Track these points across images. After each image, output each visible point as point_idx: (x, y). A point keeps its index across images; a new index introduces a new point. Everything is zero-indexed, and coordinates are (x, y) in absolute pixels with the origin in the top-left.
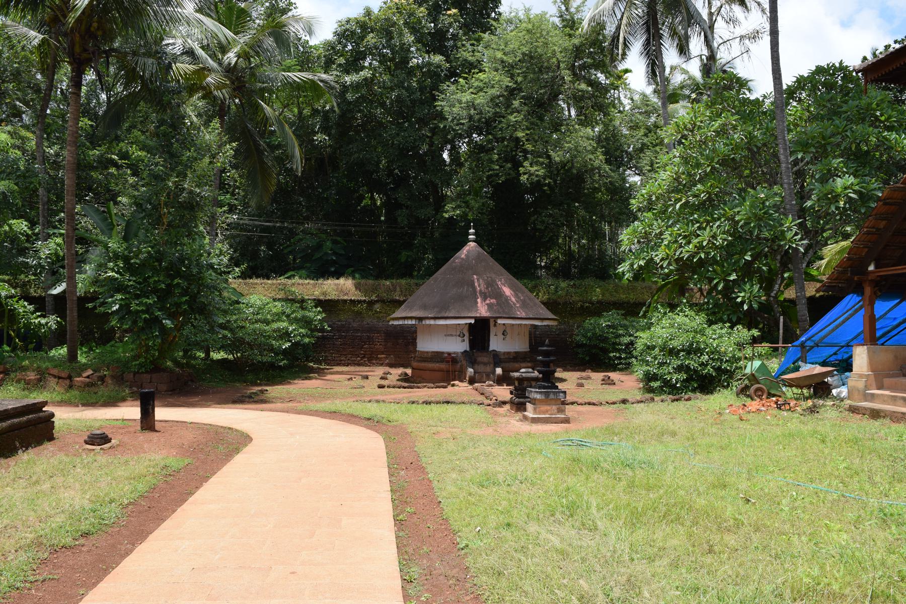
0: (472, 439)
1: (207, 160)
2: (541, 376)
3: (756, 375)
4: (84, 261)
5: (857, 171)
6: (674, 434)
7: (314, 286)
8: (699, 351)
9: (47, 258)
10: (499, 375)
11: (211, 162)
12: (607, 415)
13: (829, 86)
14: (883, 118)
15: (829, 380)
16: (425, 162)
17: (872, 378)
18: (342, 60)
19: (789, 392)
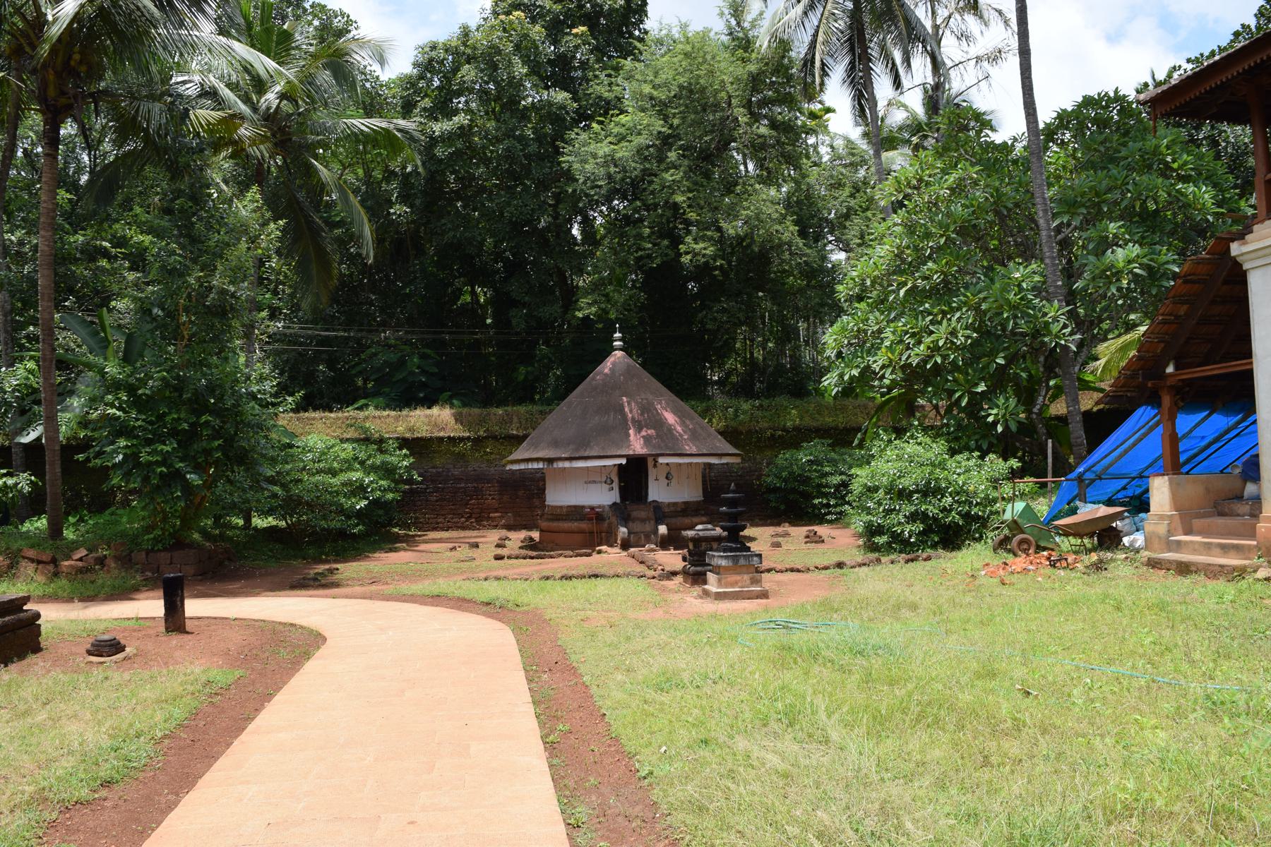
0: (638, 626)
1: (243, 245)
2: (726, 533)
3: (1020, 521)
4: (71, 393)
5: (1143, 238)
6: (914, 607)
7: (397, 419)
8: (939, 492)
9: (14, 391)
10: (663, 536)
11: (249, 248)
12: (817, 584)
13: (1102, 123)
14: (1175, 166)
15: (1118, 524)
16: (547, 241)
17: (1177, 519)
18: (427, 103)
19: (1065, 543)
